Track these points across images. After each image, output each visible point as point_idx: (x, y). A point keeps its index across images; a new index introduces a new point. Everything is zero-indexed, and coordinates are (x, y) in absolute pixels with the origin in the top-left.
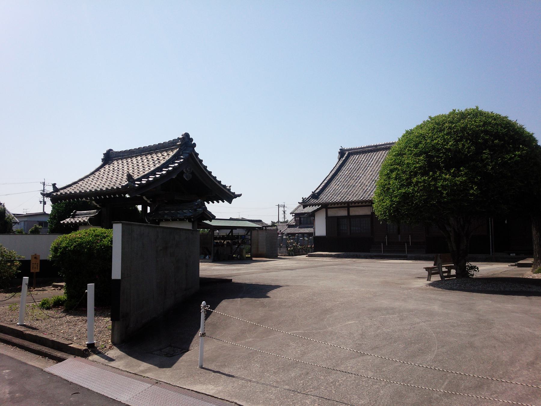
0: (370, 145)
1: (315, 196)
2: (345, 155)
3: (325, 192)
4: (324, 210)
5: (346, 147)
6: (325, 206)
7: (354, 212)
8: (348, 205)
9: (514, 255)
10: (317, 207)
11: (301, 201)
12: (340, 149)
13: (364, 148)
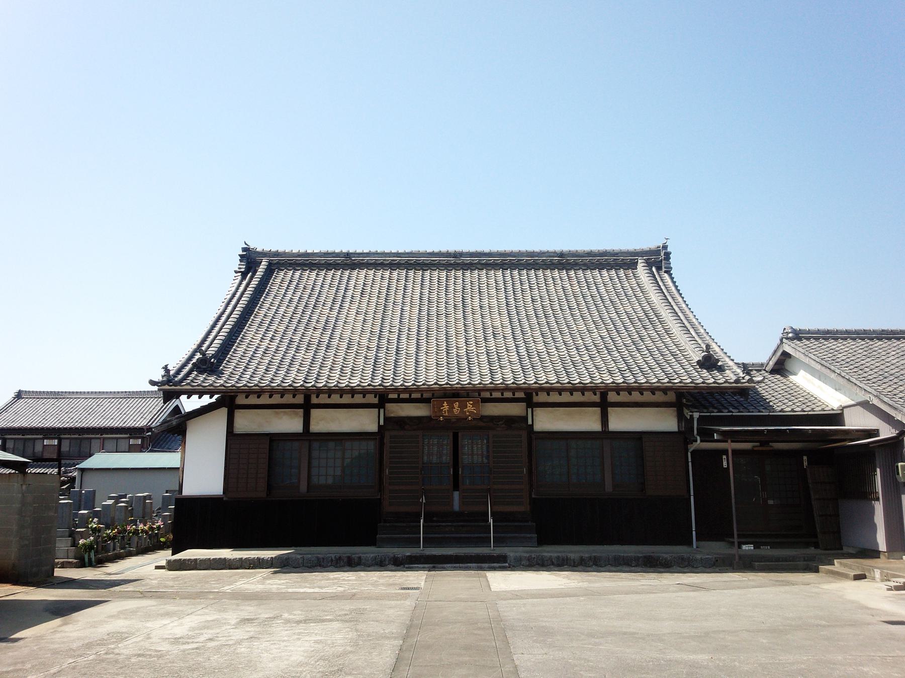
0: (330, 250)
1: (207, 363)
2: (19, 395)
3: (239, 350)
4: (223, 412)
5: (259, 245)
6: (229, 401)
7: (326, 422)
8: (306, 400)
9: (751, 547)
10: (206, 400)
11: (158, 377)
12: (244, 250)
13: (313, 254)
